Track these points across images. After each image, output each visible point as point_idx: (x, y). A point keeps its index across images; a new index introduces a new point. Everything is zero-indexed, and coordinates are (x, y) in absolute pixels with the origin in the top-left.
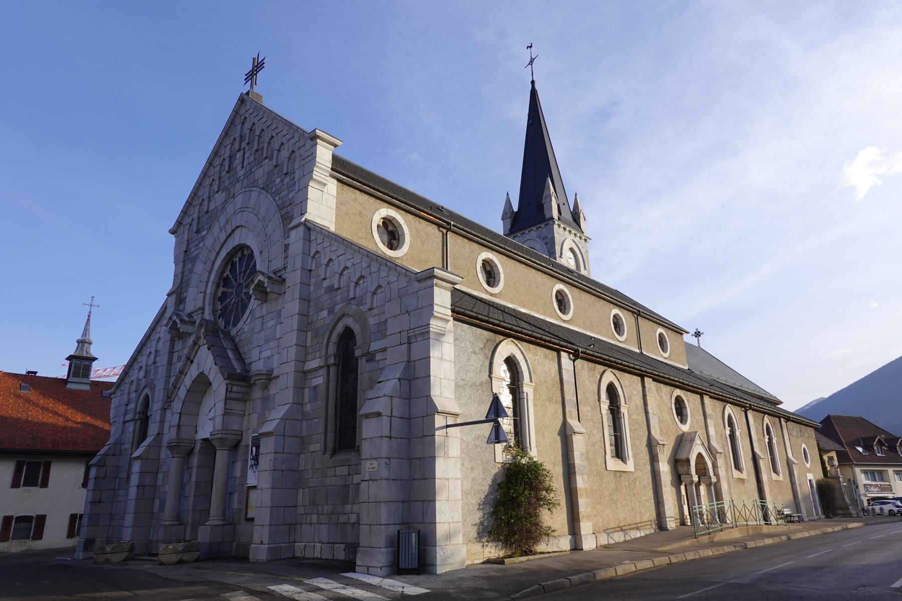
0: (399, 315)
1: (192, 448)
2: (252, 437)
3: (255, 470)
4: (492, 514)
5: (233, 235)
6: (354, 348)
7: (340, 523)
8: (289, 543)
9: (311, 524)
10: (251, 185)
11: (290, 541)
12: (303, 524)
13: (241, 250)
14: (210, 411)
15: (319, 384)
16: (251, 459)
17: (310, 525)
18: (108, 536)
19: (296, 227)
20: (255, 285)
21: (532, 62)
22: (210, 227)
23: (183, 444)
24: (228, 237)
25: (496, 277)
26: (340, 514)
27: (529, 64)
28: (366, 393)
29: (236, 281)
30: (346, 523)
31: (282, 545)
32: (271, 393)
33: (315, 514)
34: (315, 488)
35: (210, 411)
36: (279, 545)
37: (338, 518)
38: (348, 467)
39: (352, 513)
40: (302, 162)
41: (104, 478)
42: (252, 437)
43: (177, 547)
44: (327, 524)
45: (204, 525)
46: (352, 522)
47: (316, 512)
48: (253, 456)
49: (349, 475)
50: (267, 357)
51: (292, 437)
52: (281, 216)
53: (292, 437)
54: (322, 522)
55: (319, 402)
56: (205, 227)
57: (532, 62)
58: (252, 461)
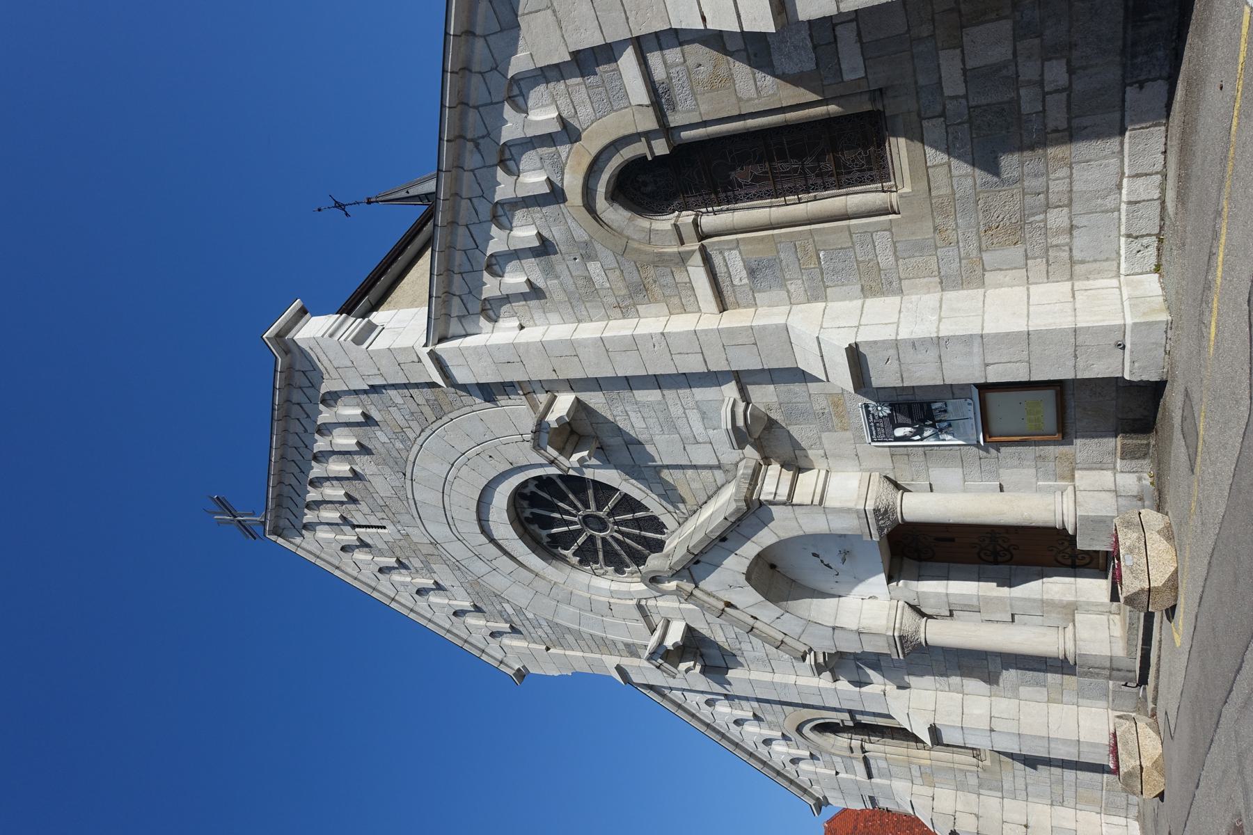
0: (554, 11)
1: (906, 605)
2: (873, 441)
3: (946, 424)
4: (1054, 603)
5: (500, 542)
6: (650, 158)
7: (1069, 120)
8: (1120, 288)
9: (1072, 227)
10: (405, 502)
11: (1118, 285)
12: (1071, 257)
13: (526, 524)
14: (827, 566)
15: (742, 259)
16: (922, 440)
17: (1075, 233)
18: (1097, 813)
19: (442, 369)
20: (561, 453)
21: (339, 206)
22: (496, 595)
23: (898, 621)
24: (506, 553)
25: (794, 578)
26: (1045, 126)
27: (336, 202)
28: (745, 97)
29: (579, 532)
30: (1069, 96)
31: (1125, 297)
32: (775, 399)
33: (1045, 221)
34: (982, 229)
35: (827, 566)
36: (1126, 304)
37: (1056, 131)
38: (925, 123)
39: (1041, 83)
40: (334, 377)
41: (977, 817)
42: (873, 441)
43: (1127, 544)
44: (1071, 168)
45: (1074, 536)
46: (1066, 76)
47: (1042, 216)
48: (915, 434)
49: (943, 114)
50: (703, 419)
51: (862, 313)
52: (437, 419)
53: (862, 313)
54: (1065, 188)
55: (782, 256)
56: (499, 607)
57: (339, 206)
58: (926, 434)
